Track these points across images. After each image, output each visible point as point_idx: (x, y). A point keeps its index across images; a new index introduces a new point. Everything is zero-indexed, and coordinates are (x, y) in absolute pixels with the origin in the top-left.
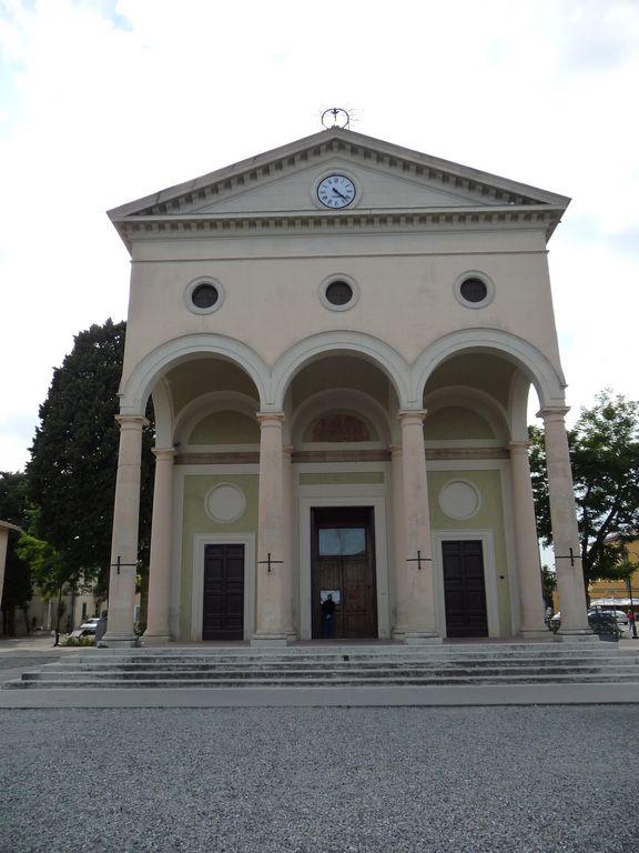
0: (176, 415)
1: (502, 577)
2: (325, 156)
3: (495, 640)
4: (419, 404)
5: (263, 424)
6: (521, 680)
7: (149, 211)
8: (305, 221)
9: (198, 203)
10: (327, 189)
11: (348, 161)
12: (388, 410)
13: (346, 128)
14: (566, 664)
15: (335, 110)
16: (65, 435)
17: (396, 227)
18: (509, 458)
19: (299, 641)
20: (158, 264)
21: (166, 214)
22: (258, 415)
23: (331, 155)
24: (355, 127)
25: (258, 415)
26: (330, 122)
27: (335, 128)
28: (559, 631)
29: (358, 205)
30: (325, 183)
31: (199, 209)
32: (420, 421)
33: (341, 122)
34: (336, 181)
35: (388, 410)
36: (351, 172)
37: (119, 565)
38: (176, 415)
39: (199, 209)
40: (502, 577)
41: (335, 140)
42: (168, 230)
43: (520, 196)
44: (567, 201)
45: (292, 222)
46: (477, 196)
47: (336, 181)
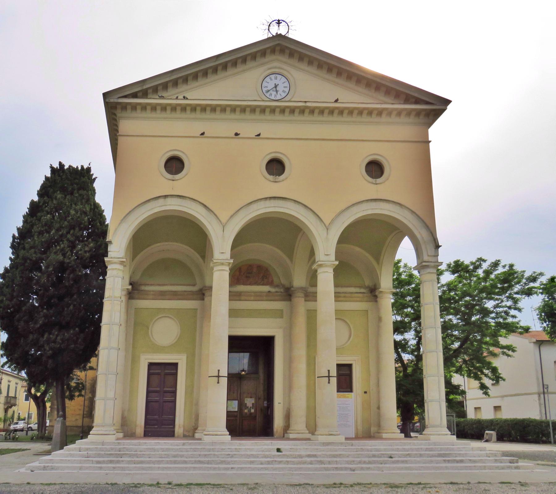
0: (133, 260)
1: (365, 392)
2: (269, 58)
3: (179, 438)
4: (228, 255)
5: (109, 267)
6: (170, 468)
7: (135, 95)
8: (253, 110)
9: (172, 92)
10: (270, 84)
11: (285, 63)
12: (204, 262)
13: (287, 35)
14: (263, 457)
15: (279, 21)
16: (397, 279)
17: (213, 116)
18: (376, 301)
19: (129, 434)
20: (139, 138)
21: (147, 98)
22: (106, 259)
23: (273, 57)
24: (291, 36)
25: (106, 259)
26: (275, 30)
27: (279, 36)
28: (316, 433)
29: (293, 97)
30: (268, 79)
31: (169, 96)
32: (227, 268)
33: (283, 30)
34: (276, 78)
35: (378, 263)
36: (288, 72)
37: (329, 377)
38: (133, 260)
39: (169, 96)
40: (365, 392)
41: (278, 45)
42: (159, 111)
43: (414, 97)
44: (447, 102)
45: (243, 110)
46: (381, 97)
47: (276, 78)
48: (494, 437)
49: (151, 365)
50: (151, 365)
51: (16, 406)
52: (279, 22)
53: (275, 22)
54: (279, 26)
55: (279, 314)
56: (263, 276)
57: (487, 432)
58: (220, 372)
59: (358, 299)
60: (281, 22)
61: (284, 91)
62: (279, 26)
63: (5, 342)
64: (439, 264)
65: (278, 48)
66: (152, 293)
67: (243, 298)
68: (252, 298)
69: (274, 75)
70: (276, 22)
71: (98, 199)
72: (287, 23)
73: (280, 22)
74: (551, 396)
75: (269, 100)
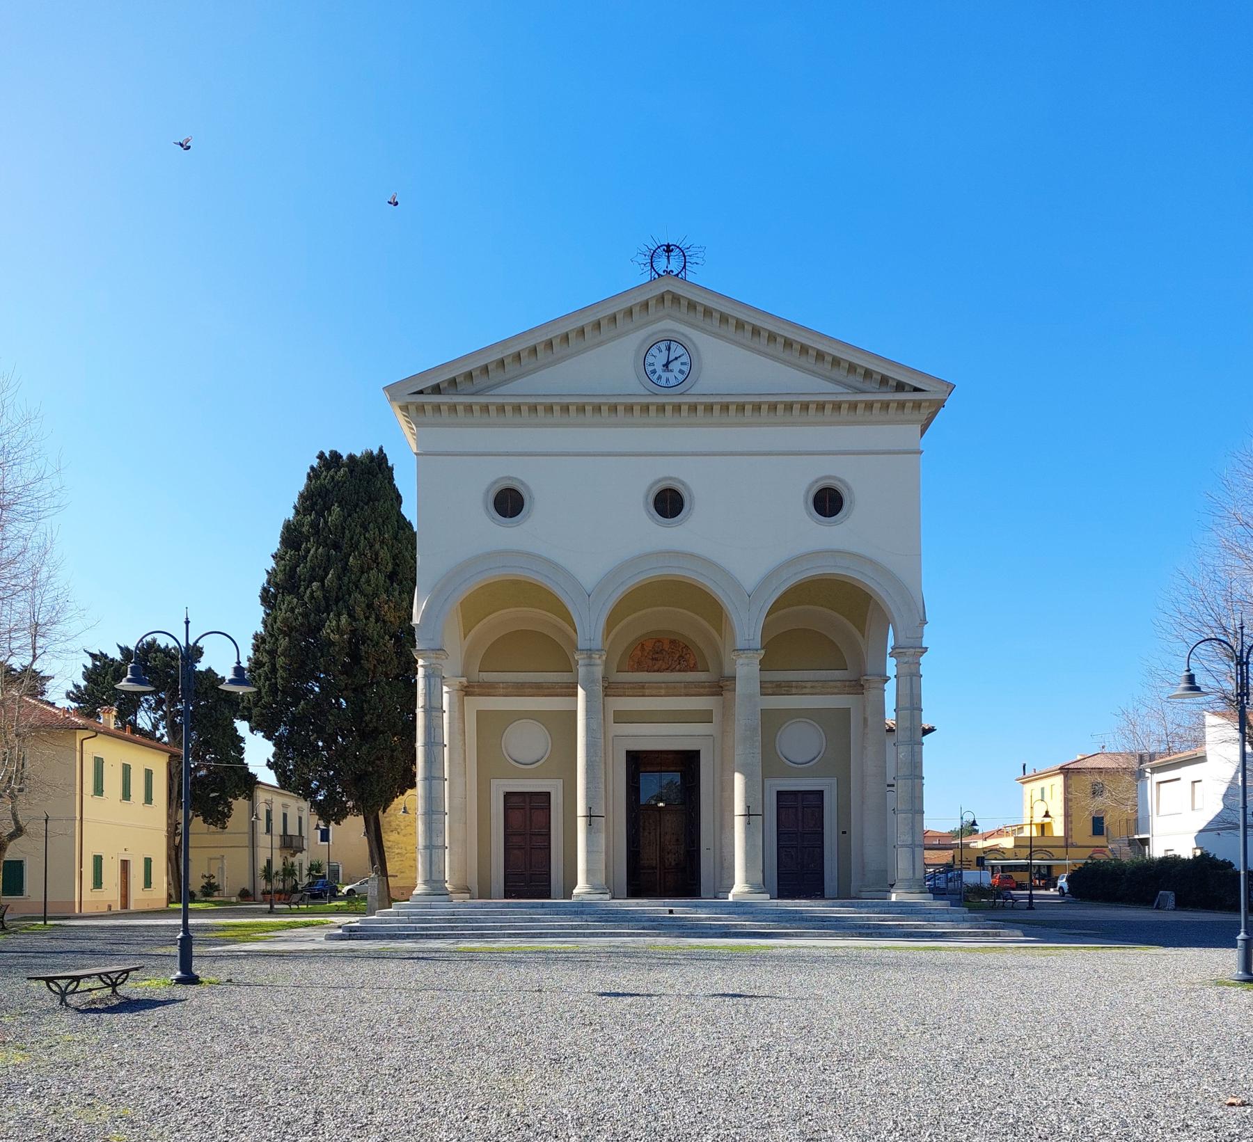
15: (668, 246)
34: (654, 372)
40: (844, 833)
48: (1171, 902)
49: (508, 796)
50: (508, 796)
51: (304, 852)
52: (668, 249)
53: (662, 248)
54: (668, 257)
55: (704, 717)
56: (679, 657)
57: (1161, 892)
58: (1026, 767)
59: (836, 691)
60: (673, 250)
61: (681, 372)
62: (668, 257)
63: (262, 734)
64: (923, 650)
65: (668, 298)
66: (501, 685)
67: (647, 692)
68: (663, 692)
69: (664, 342)
70: (664, 250)
71: (404, 510)
72: (682, 251)
73: (671, 248)
74: (246, 830)
75: (650, 393)
